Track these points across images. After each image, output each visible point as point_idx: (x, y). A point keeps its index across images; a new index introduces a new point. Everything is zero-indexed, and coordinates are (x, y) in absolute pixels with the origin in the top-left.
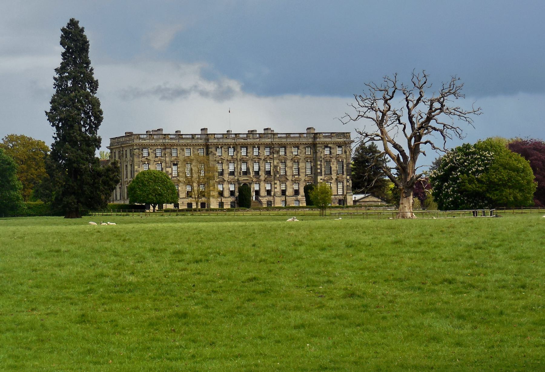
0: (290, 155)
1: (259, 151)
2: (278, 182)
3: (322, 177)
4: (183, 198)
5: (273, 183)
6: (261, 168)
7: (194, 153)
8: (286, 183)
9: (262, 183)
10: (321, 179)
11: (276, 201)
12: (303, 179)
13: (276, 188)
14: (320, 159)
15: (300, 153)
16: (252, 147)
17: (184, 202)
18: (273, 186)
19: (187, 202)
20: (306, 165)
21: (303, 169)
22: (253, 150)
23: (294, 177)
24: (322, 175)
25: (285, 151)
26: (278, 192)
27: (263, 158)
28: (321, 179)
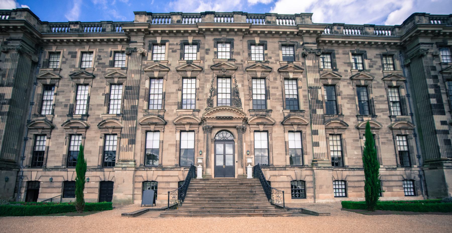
0: (346, 71)
1: (266, 52)
2: (321, 130)
3: (445, 118)
4: (56, 168)
5: (307, 131)
6: (272, 91)
7: (100, 61)
8: (340, 135)
9: (277, 130)
10: (443, 123)
11: (318, 183)
12: (385, 126)
13: (316, 144)
14: (433, 73)
15: (371, 66)
16: (245, 44)
17: (55, 179)
18: (308, 138)
19: (61, 179)
20: (388, 94)
21: (382, 102)
22: (250, 49)
23: (363, 120)
24: (443, 113)
25: (331, 62)
26: (323, 154)
27: (276, 67)
28: (443, 123)
